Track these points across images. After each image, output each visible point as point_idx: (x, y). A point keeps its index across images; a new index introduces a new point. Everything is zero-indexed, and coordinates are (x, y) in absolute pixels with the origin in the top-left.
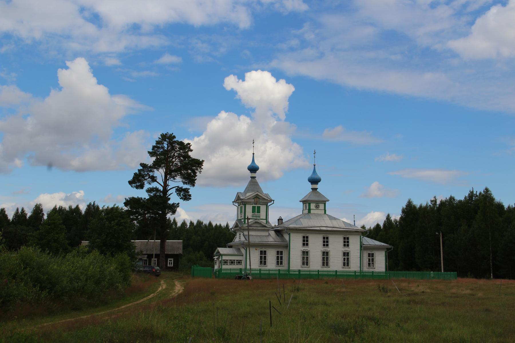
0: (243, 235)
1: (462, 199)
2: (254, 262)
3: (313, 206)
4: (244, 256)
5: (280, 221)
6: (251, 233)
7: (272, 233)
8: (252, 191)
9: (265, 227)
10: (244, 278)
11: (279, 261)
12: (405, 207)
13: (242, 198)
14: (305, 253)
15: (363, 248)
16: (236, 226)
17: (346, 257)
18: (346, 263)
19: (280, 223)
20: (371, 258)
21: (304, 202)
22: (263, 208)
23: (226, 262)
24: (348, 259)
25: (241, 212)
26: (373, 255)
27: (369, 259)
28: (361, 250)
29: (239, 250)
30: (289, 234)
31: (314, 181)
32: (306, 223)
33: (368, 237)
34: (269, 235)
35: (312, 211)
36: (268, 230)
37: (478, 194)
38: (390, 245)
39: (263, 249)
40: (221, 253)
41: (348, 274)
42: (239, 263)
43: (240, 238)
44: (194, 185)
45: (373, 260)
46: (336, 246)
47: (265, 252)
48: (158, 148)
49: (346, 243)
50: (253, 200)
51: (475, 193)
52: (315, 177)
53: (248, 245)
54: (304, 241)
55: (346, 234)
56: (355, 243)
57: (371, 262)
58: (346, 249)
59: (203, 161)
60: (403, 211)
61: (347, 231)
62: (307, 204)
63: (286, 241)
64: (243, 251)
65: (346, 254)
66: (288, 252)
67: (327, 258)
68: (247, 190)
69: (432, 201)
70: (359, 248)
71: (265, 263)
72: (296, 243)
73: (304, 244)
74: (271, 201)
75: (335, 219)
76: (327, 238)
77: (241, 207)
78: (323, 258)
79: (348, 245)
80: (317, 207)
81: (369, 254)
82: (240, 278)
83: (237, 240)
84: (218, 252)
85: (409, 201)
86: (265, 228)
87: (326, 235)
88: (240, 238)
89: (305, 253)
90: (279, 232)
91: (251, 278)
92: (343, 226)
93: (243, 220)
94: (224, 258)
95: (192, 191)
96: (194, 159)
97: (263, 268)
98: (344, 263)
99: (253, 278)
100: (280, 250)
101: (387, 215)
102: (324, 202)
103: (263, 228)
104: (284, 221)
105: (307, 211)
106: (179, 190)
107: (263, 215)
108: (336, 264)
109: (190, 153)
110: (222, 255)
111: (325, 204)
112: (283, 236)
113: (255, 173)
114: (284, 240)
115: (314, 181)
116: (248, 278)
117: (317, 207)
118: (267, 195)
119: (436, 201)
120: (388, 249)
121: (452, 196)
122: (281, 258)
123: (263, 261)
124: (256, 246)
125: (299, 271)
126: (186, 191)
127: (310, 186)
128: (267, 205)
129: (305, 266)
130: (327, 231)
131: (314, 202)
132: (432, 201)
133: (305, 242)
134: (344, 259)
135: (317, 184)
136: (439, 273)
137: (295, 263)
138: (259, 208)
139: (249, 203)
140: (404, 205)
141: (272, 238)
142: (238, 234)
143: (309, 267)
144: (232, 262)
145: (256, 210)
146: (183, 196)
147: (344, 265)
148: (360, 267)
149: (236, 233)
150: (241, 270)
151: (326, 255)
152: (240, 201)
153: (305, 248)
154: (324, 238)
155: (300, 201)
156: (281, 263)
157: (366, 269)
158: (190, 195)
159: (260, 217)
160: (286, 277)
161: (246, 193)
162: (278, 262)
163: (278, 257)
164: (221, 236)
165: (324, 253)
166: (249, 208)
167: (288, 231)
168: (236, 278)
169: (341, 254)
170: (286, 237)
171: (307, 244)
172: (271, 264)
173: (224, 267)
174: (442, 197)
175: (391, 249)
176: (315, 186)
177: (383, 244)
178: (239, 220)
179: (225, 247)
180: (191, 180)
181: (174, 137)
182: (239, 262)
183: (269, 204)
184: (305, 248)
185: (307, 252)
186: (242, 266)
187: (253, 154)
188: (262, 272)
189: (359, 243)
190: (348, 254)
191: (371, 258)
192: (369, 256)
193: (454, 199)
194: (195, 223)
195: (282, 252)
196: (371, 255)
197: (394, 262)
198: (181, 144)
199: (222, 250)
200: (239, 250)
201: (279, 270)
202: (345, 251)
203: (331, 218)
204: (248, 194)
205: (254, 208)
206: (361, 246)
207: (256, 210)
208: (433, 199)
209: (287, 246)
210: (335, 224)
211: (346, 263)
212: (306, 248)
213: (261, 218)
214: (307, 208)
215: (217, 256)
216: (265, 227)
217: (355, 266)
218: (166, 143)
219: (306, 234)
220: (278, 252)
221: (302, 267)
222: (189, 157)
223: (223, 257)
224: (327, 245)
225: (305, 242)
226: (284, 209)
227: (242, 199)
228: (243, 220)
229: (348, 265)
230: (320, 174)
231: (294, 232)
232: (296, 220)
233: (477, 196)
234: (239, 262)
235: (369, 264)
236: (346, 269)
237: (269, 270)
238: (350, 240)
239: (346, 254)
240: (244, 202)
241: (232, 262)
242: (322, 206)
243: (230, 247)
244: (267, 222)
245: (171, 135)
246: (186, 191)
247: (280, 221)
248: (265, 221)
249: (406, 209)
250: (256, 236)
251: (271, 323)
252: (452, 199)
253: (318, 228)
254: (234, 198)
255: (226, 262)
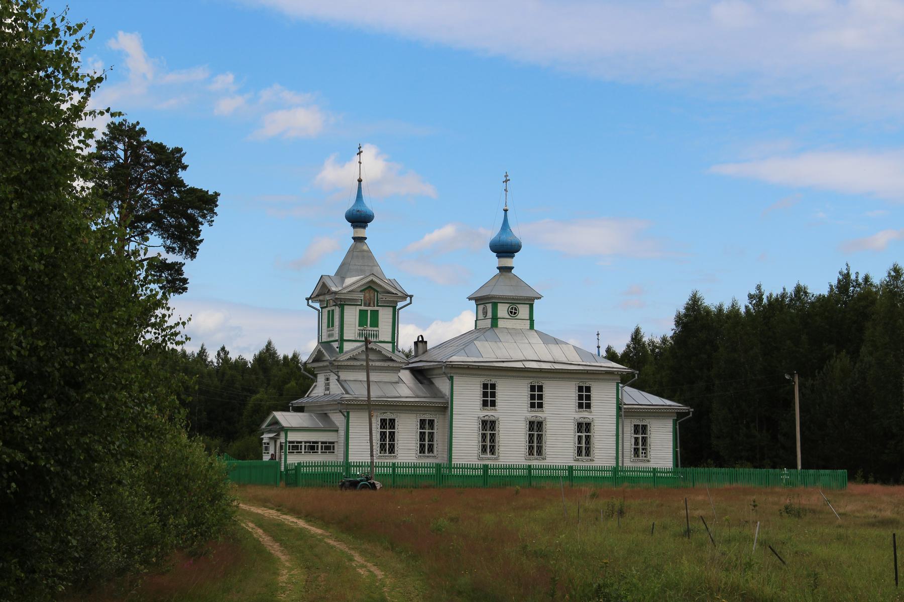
0: (338, 380)
1: (825, 292)
2: (360, 446)
3: (503, 310)
4: (342, 433)
5: (420, 345)
6: (374, 377)
7: (405, 375)
8: (360, 272)
9: (389, 363)
10: (364, 487)
11: (426, 446)
12: (683, 311)
13: (334, 289)
14: (489, 426)
15: (623, 412)
16: (318, 357)
17: (583, 435)
18: (584, 448)
19: (420, 350)
20: (640, 436)
21: (479, 300)
22: (385, 315)
23: (295, 447)
24: (588, 438)
25: (331, 324)
26: (644, 428)
27: (636, 439)
28: (618, 416)
29: (325, 416)
30: (451, 379)
31: (505, 249)
32: (489, 352)
33: (633, 386)
34: (400, 380)
35: (501, 323)
36: (398, 369)
37: (860, 280)
38: (685, 403)
39: (388, 416)
40: (284, 424)
41: (598, 474)
42: (328, 448)
43: (327, 389)
44: (193, 256)
45: (644, 440)
46: (560, 406)
47: (392, 421)
48: (103, 159)
49: (584, 402)
50: (361, 297)
51: (853, 277)
52: (506, 238)
53: (347, 407)
54: (485, 394)
55: (583, 382)
56: (604, 400)
57: (641, 446)
58: (584, 415)
59: (217, 194)
60: (679, 321)
61: (587, 372)
62: (489, 307)
63: (443, 397)
64: (338, 419)
65: (584, 427)
66: (447, 425)
67: (540, 437)
68: (342, 272)
69: (751, 297)
70: (614, 411)
71: (392, 450)
72: (466, 400)
73: (485, 404)
74: (405, 296)
75: (556, 342)
76: (540, 388)
77: (331, 315)
78: (531, 437)
79: (588, 406)
80: (513, 313)
81: (636, 427)
82: (354, 485)
83: (318, 391)
84: (276, 422)
85: (694, 296)
86: (391, 364)
87: (537, 381)
88: (327, 389)
89: (489, 426)
90: (422, 375)
91: (378, 485)
92: (575, 358)
93: (335, 345)
94: (293, 437)
95: (190, 269)
96: (193, 190)
97: (535, 463)
98: (579, 449)
99: (384, 486)
100: (427, 417)
101: (633, 330)
102: (529, 302)
103: (386, 364)
104: (429, 346)
105: (488, 323)
106: (158, 266)
107: (384, 332)
108: (560, 451)
109: (181, 174)
110: (286, 430)
111: (531, 306)
112: (432, 383)
113: (364, 227)
114: (436, 393)
115: (505, 249)
116: (373, 486)
117: (513, 313)
118: (392, 283)
119: (761, 299)
120: (680, 415)
121: (802, 284)
122: (431, 435)
123: (388, 444)
124: (368, 406)
125: (571, 469)
126: (176, 268)
127: (493, 262)
128: (394, 308)
129: (489, 456)
130: (541, 371)
131: (503, 303)
132: (751, 297)
133: (489, 398)
134: (580, 438)
135: (513, 257)
136: (793, 471)
137: (465, 449)
138: (375, 314)
139: (353, 303)
140: (680, 304)
141: (405, 388)
142: (321, 379)
143: (496, 459)
144: (312, 447)
145: (369, 319)
146: (168, 282)
147: (579, 452)
148: (617, 458)
149: (315, 376)
150: (438, 467)
151: (536, 428)
152: (328, 297)
153: (489, 413)
154: (532, 388)
155: (470, 299)
156: (431, 449)
157: (628, 462)
158: (185, 281)
159: (377, 336)
160: (442, 481)
161: (343, 279)
162: (422, 447)
163: (422, 435)
164: (276, 380)
165: (531, 424)
166: (352, 315)
167: (448, 371)
168: (343, 485)
169: (573, 427)
170: (442, 385)
171: (493, 404)
172: (407, 452)
173: (293, 459)
174: (777, 285)
175: (688, 413)
176: (507, 262)
177: (668, 402)
178: (325, 345)
179: (286, 409)
180: (187, 240)
181: (143, 132)
182: (328, 447)
183: (400, 305)
184: (489, 413)
185: (493, 423)
186: (337, 457)
187: (360, 181)
188: (399, 471)
189: (614, 401)
190: (493, 423)
191: (640, 436)
192: (636, 432)
193: (806, 293)
194: (290, 356)
195: (431, 422)
196: (640, 430)
197: (693, 449)
198: (158, 149)
199: (285, 418)
200: (325, 416)
201: (486, 467)
202: (581, 420)
203: (547, 339)
204: (349, 281)
205: (363, 314)
206: (619, 408)
207: (369, 319)
208: (754, 291)
209: (445, 408)
210: (566, 356)
211: (584, 448)
212: (490, 413)
213: (381, 339)
214: (490, 315)
215: (270, 432)
216: (391, 360)
217: (604, 454)
218: (121, 146)
219: (490, 379)
220: (422, 422)
221: (480, 459)
222: (181, 183)
223: (289, 434)
224: (540, 406)
225: (489, 398)
226: (437, 320)
227: (336, 293)
228: (335, 345)
229: (588, 453)
230: (518, 232)
231: (462, 375)
232: (465, 341)
233: (859, 285)
234: (328, 447)
235: (636, 451)
236: (584, 463)
237: (510, 468)
238: (594, 394)
239: (584, 427)
240: (341, 299)
241: (312, 447)
242: (523, 311)
243: (300, 409)
244: (395, 347)
245: (134, 126)
246: (176, 268)
247: (420, 345)
248: (389, 347)
249: (685, 315)
250: (356, 384)
251: (896, 579)
252: (800, 291)
253: (519, 365)
254: (310, 288)
255: (295, 447)
